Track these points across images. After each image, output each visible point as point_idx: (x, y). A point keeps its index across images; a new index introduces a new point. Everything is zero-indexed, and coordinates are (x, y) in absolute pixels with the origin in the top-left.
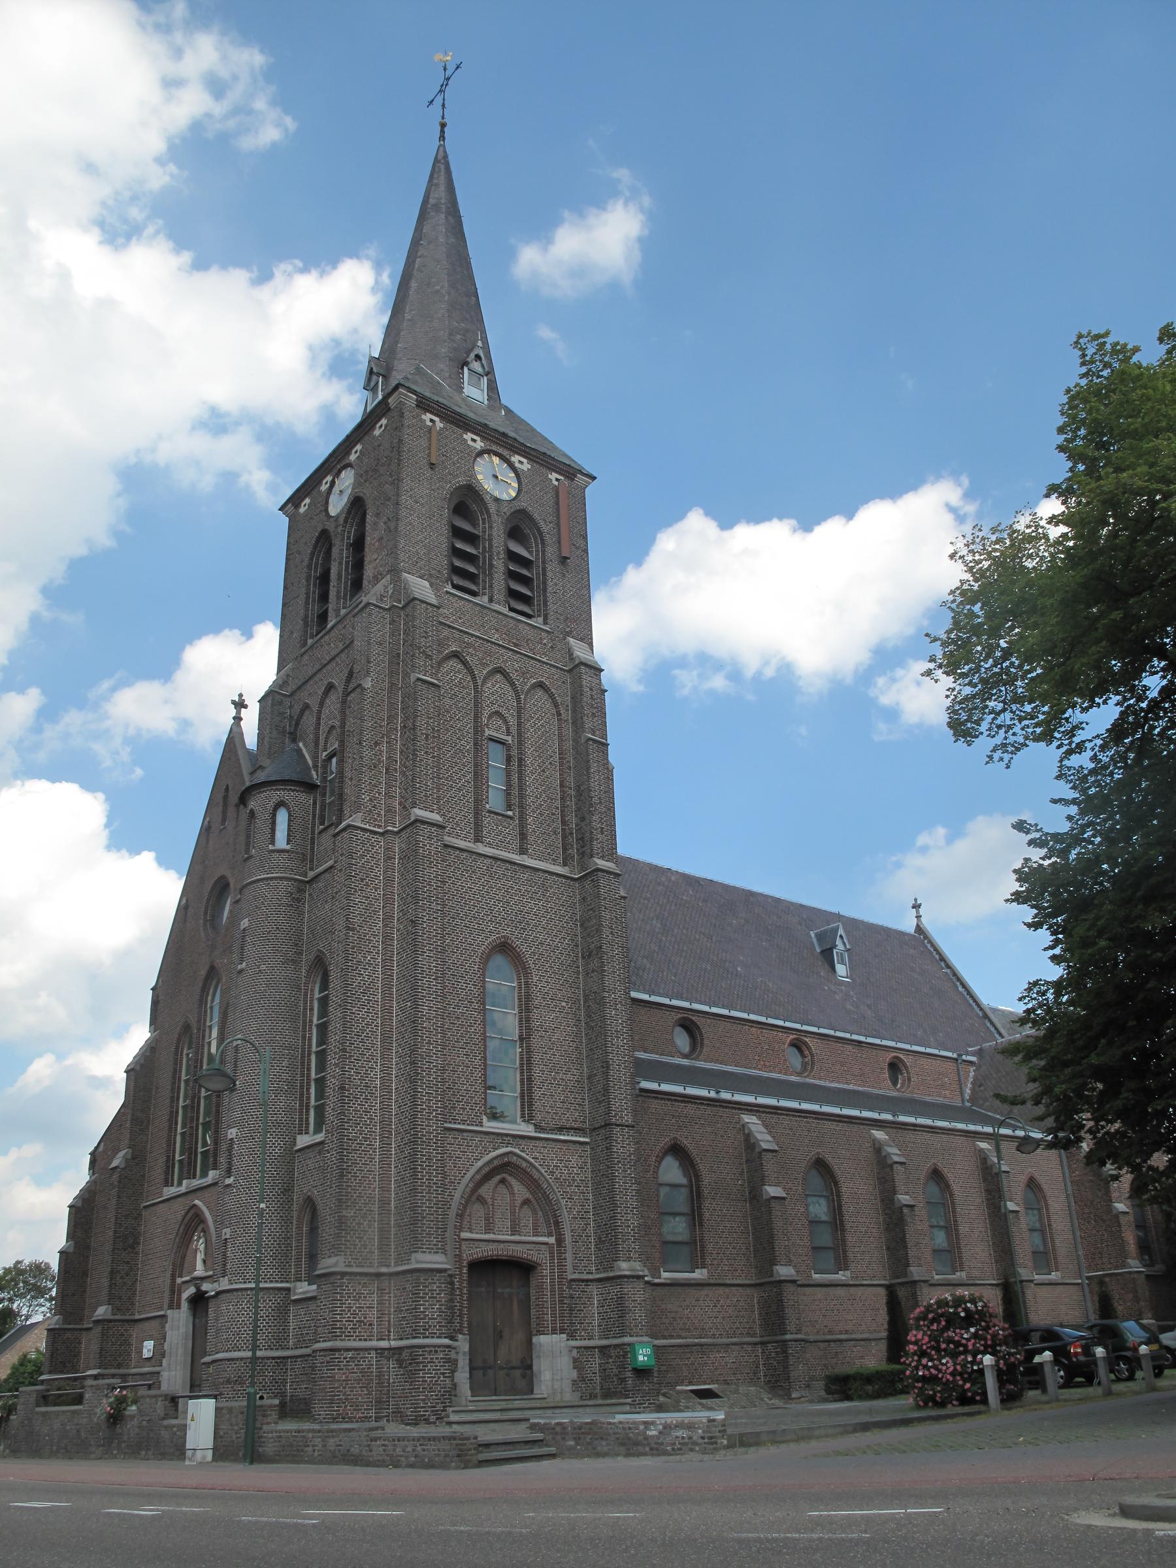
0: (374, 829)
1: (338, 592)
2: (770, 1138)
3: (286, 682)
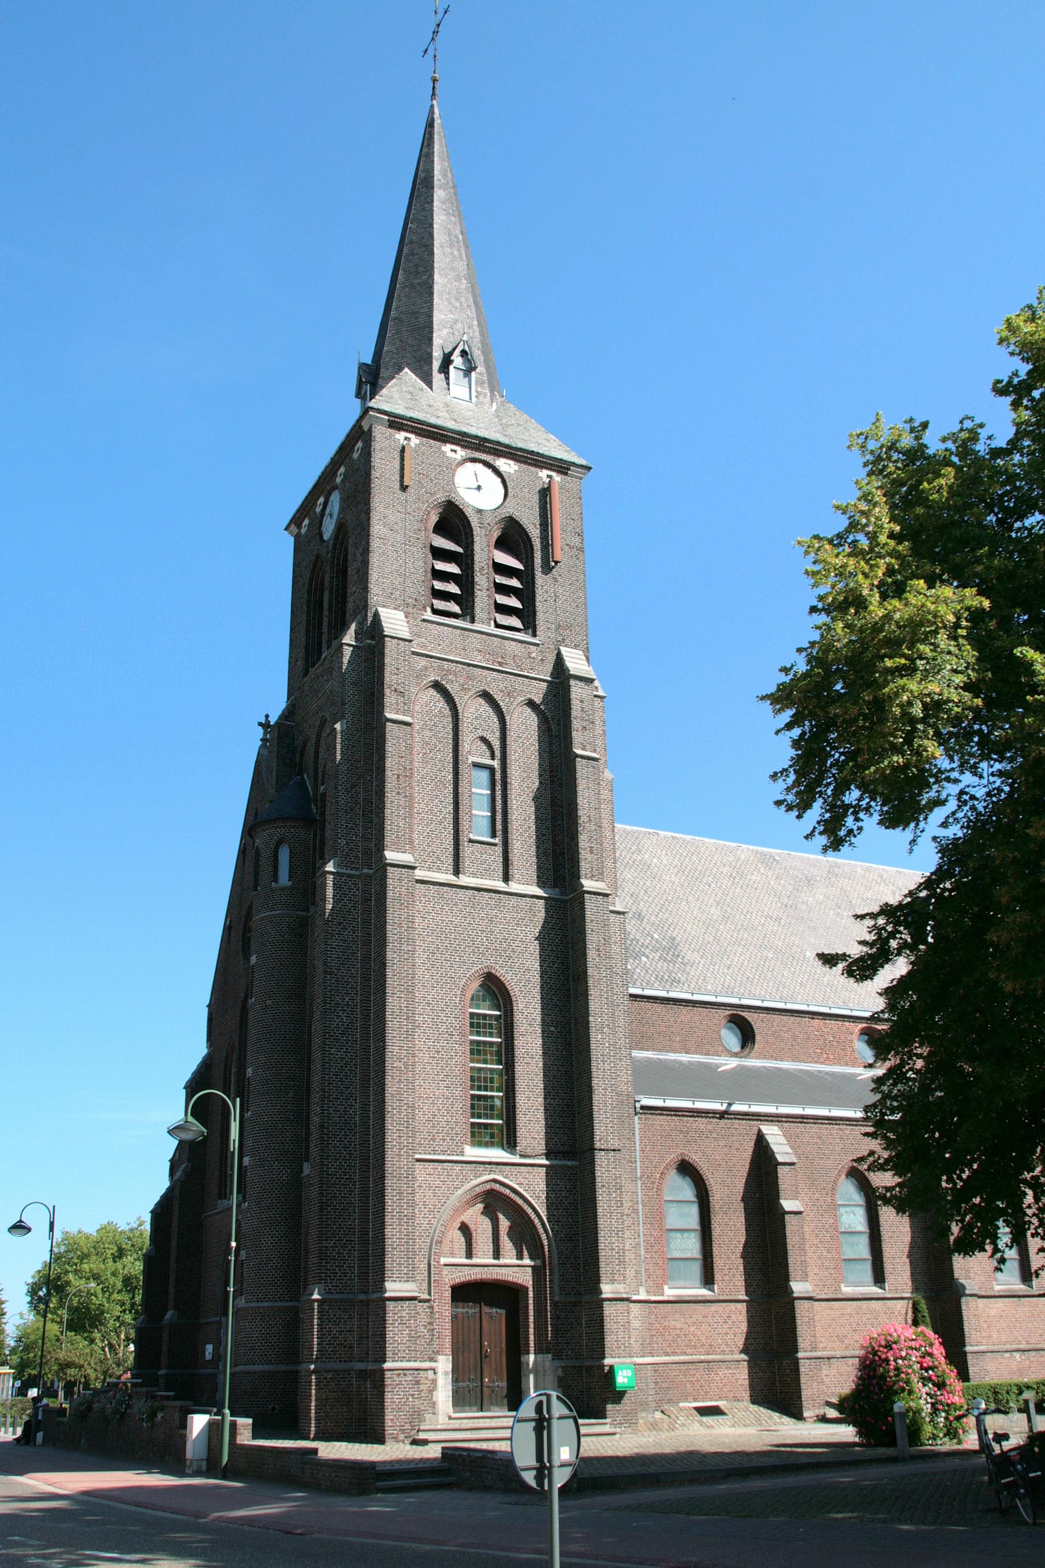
0: (351, 872)
1: (330, 622)
2: (789, 1150)
3: (292, 712)
